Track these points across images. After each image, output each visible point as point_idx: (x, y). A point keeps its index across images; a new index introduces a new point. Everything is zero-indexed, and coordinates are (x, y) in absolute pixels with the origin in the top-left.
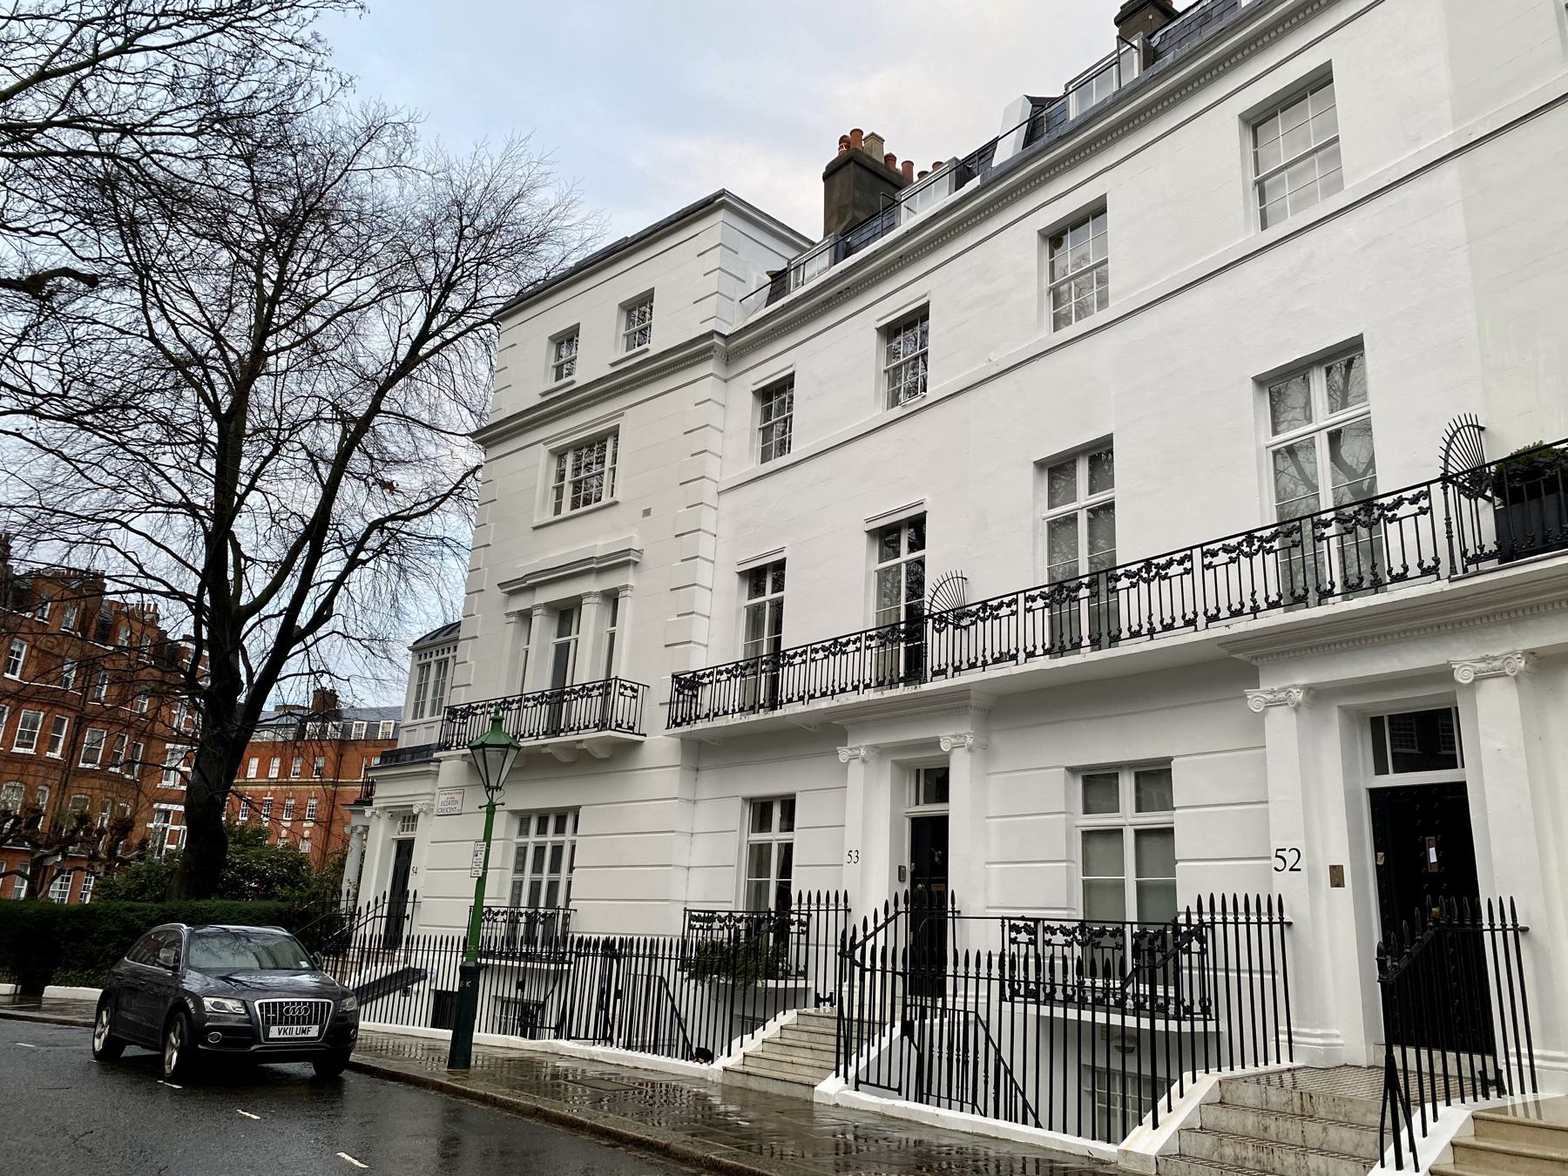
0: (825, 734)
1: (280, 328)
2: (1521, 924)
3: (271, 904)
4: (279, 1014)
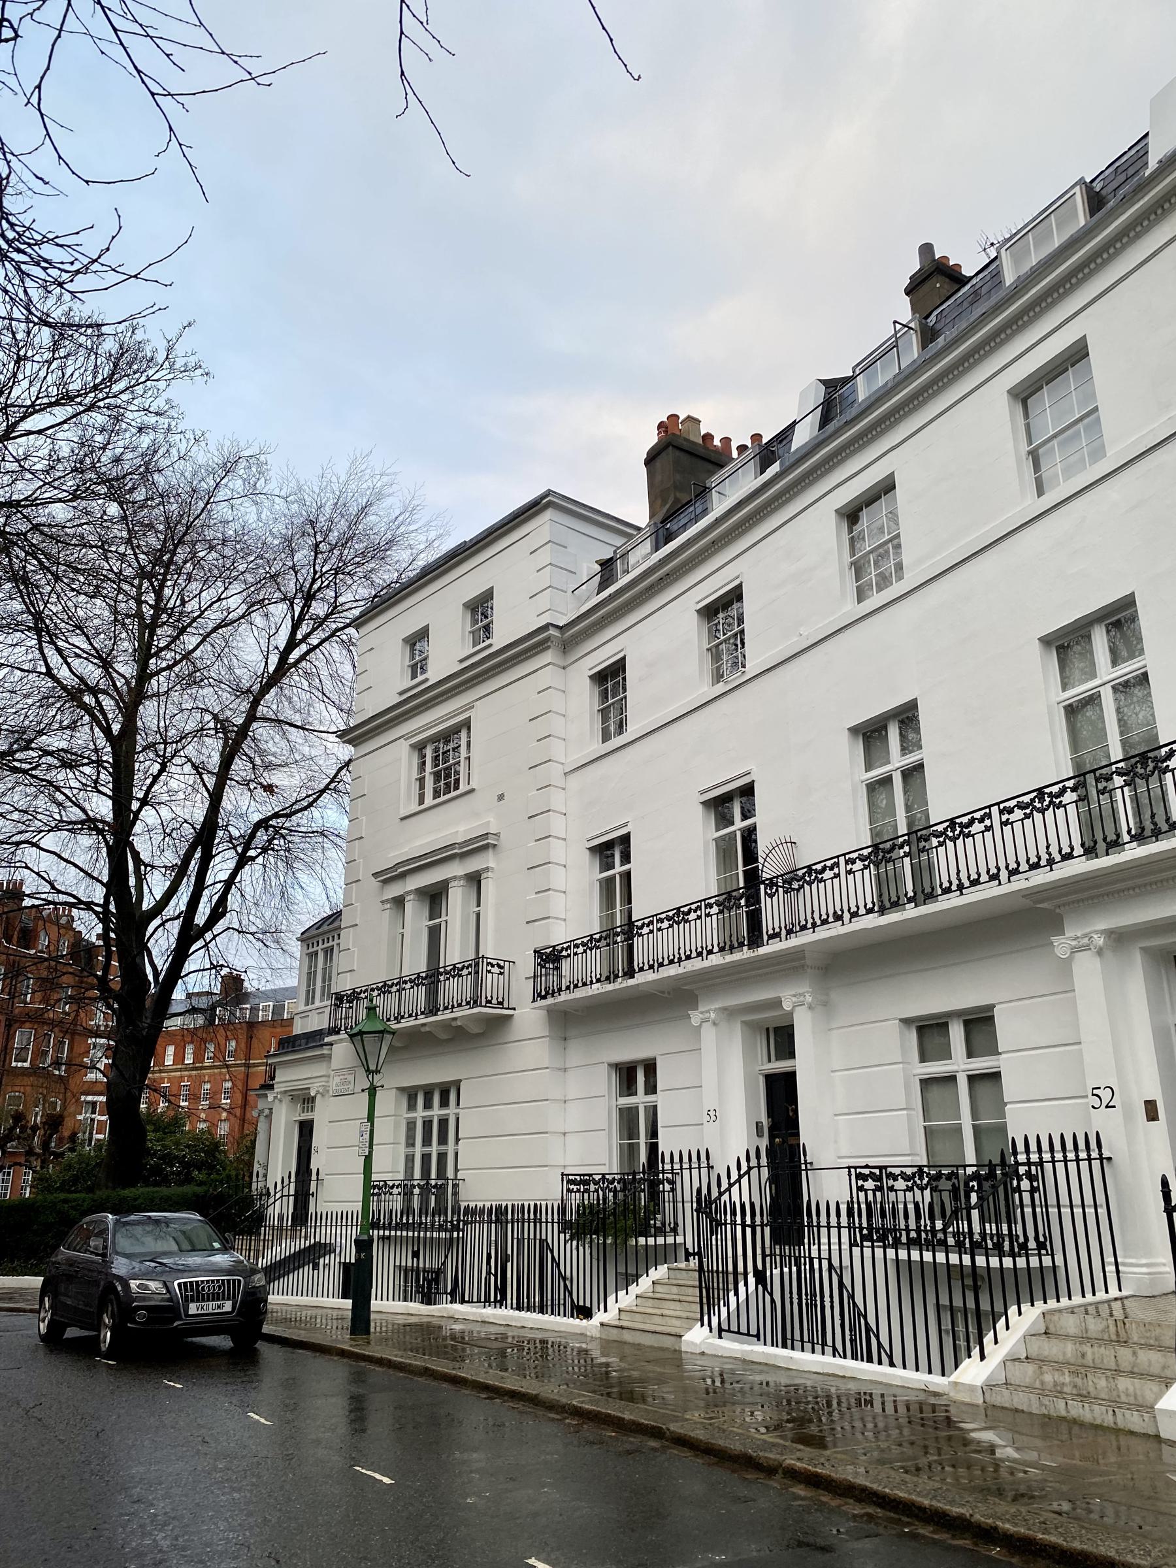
0: (676, 999)
1: (161, 650)
2: (1106, 1154)
3: (188, 1189)
4: (196, 1292)
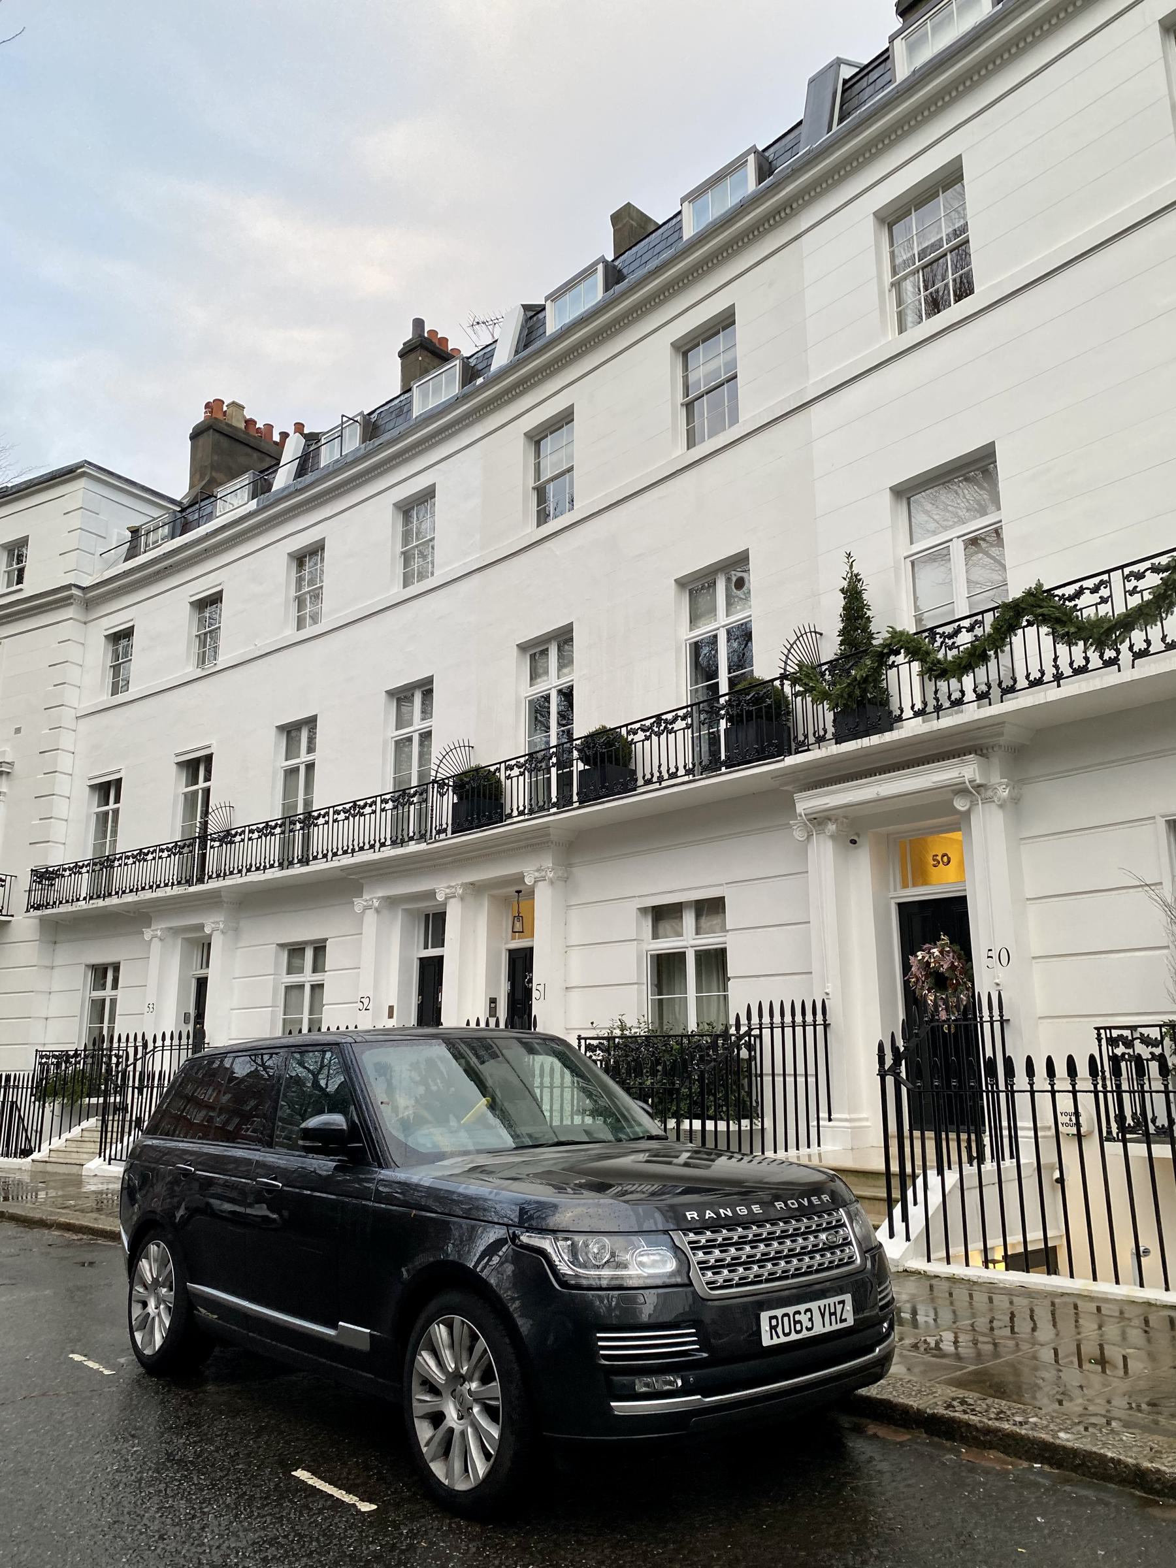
0: (341, 887)
